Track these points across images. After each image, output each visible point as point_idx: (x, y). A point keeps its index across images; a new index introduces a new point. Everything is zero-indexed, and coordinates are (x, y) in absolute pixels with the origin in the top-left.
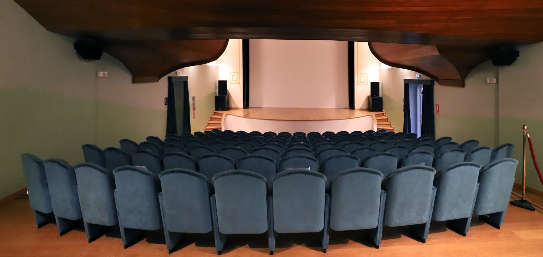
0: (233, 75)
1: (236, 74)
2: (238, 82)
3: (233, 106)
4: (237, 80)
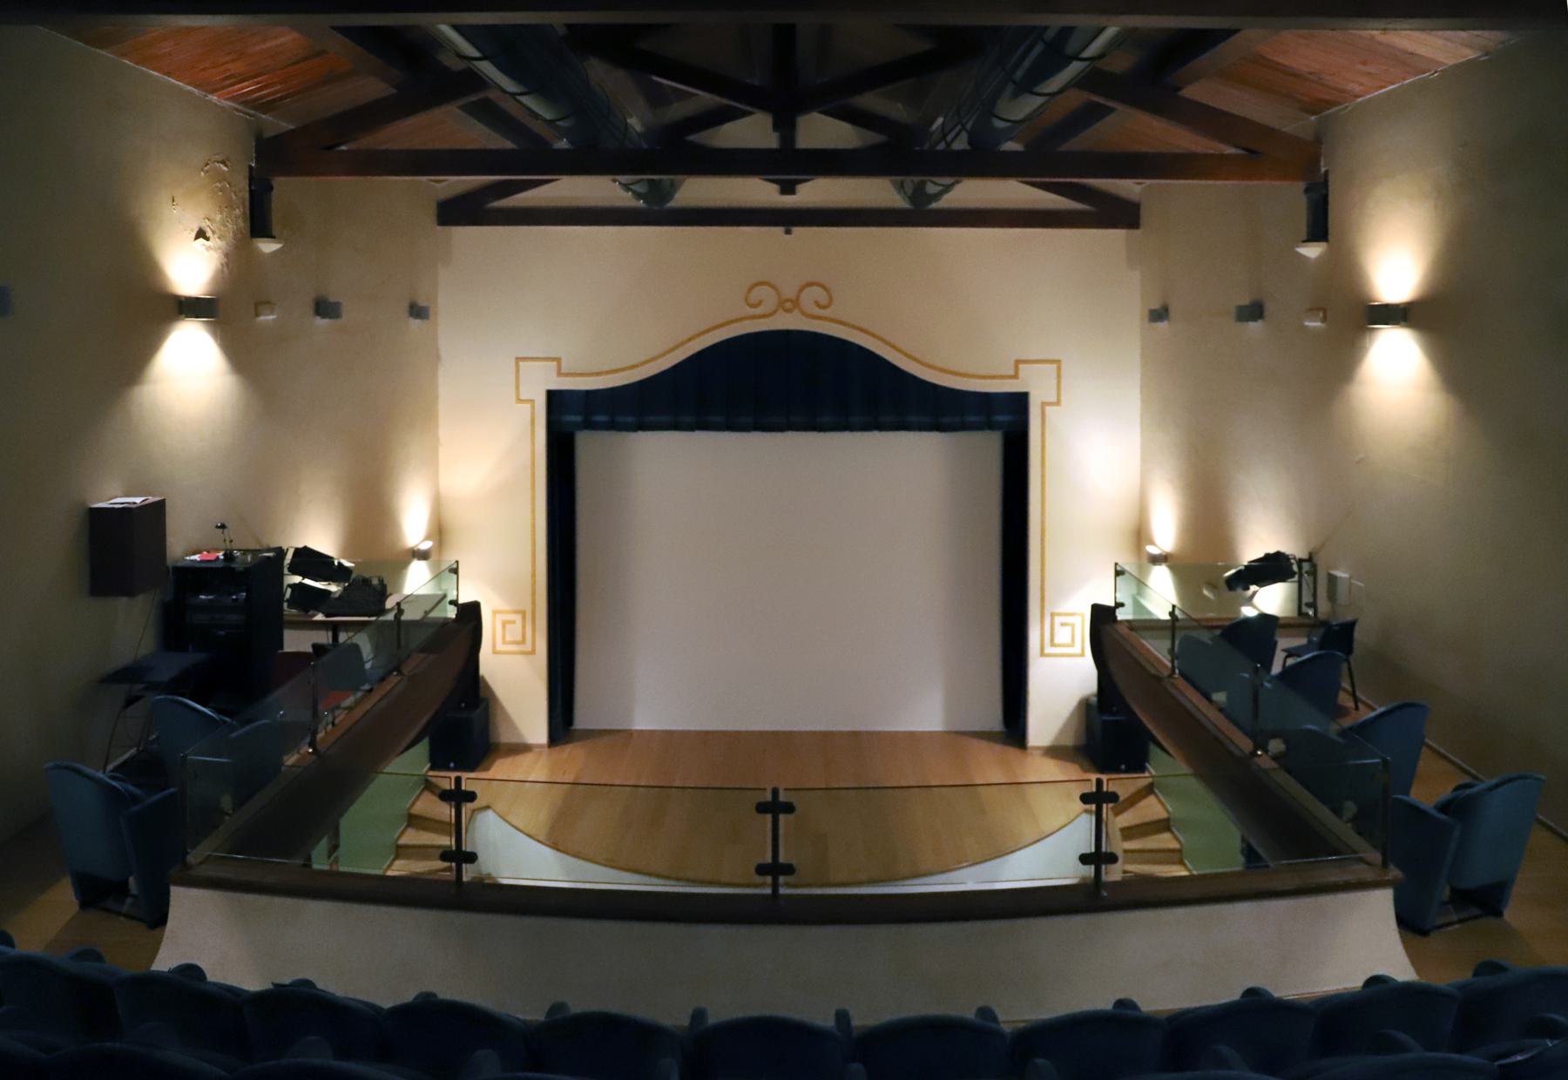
0: (504, 624)
1: (518, 618)
2: (528, 647)
3: (505, 737)
4: (523, 641)
